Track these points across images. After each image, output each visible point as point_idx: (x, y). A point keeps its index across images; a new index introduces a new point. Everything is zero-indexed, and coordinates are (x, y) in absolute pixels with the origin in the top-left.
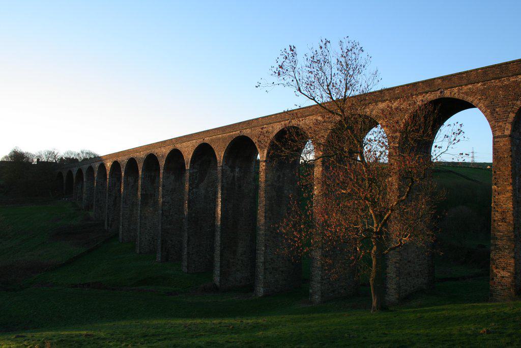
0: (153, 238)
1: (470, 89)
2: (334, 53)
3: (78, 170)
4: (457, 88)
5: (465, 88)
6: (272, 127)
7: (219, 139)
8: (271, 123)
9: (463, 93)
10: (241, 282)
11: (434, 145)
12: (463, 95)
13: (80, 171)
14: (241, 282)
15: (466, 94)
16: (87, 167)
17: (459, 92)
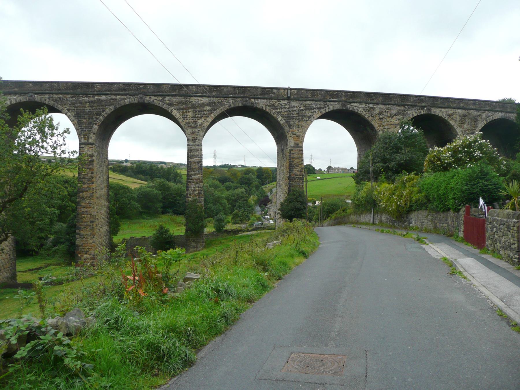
1: (60, 98)
4: (47, 95)
5: (56, 97)
9: (53, 100)
12: (53, 102)
16: (120, 232)
17: (49, 99)
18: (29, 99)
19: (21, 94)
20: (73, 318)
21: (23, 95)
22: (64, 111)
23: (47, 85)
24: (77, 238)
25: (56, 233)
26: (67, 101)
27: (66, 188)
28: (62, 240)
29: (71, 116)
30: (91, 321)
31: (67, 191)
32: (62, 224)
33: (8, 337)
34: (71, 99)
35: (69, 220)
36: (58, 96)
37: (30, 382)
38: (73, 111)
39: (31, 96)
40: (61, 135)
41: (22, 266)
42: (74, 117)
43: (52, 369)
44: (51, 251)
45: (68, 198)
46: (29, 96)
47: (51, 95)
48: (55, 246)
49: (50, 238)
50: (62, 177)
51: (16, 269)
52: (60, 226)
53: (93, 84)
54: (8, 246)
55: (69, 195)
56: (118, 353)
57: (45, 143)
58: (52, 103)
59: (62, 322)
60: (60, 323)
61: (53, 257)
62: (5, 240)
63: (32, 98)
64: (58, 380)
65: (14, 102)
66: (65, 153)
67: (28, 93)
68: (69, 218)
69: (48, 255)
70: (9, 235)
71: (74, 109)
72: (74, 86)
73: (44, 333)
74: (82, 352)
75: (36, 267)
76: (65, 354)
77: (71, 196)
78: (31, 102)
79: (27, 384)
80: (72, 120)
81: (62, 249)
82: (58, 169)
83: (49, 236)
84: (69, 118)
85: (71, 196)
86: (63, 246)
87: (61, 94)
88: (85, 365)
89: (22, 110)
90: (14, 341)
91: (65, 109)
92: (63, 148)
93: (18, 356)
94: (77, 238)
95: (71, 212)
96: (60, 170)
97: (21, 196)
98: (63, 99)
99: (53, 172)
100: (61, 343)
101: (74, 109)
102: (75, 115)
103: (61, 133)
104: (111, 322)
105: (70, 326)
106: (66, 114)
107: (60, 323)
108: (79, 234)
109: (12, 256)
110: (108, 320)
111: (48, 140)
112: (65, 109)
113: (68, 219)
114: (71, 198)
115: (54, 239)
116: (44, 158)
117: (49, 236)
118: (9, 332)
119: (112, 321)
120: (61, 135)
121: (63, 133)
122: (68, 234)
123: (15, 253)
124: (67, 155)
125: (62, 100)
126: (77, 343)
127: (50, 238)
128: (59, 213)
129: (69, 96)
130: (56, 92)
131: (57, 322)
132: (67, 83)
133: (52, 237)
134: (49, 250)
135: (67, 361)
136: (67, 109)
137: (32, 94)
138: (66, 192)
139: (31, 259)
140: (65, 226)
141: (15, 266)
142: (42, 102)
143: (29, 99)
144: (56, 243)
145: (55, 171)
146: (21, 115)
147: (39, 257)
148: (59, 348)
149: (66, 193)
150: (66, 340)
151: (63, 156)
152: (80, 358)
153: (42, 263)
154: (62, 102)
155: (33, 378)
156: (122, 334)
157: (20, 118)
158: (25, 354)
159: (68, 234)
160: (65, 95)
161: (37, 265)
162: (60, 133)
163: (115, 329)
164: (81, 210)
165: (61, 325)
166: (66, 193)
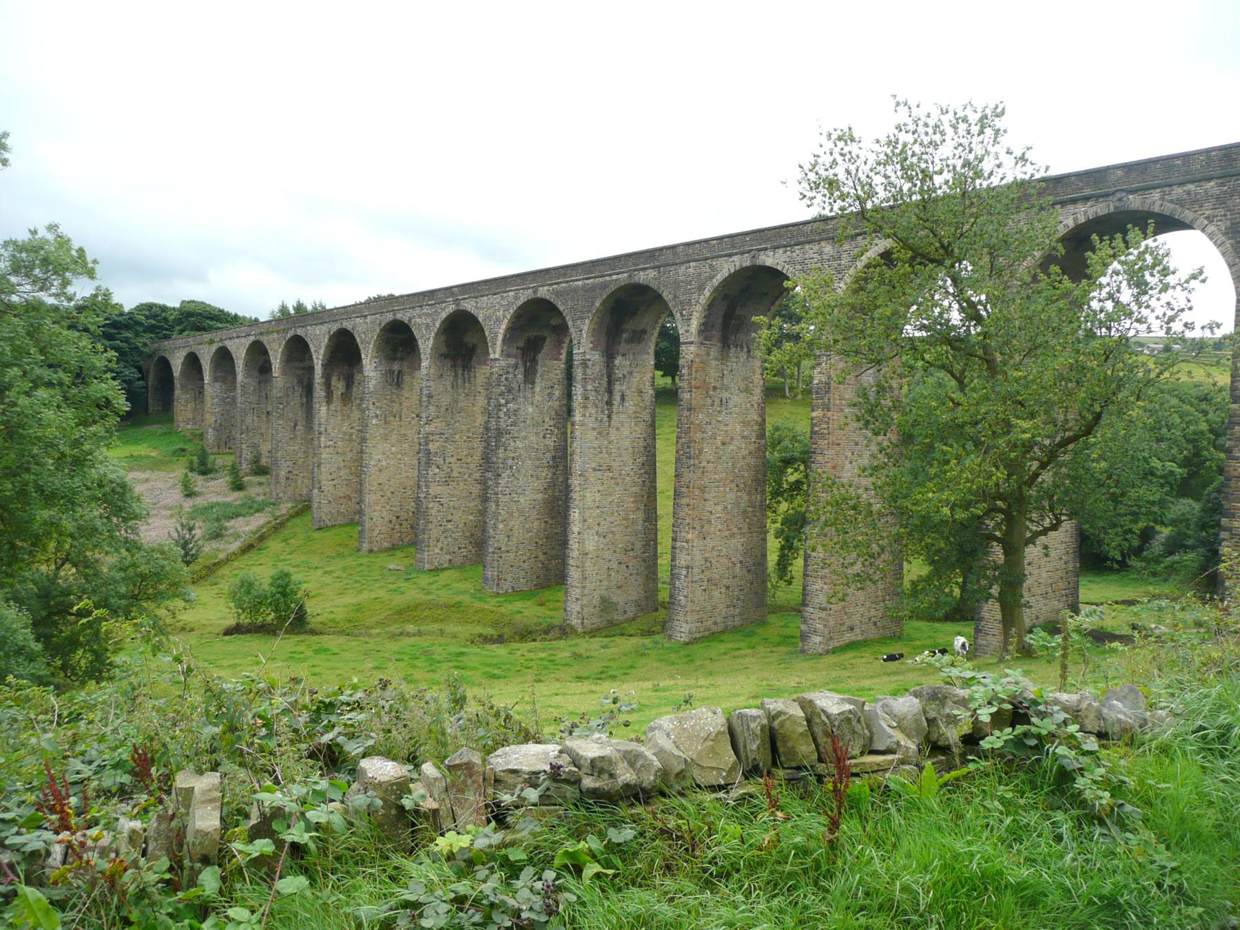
0: (398, 517)
1: (1189, 193)
2: (1166, 247)
3: (186, 357)
4: (1158, 190)
5: (1178, 191)
6: (711, 266)
7: (575, 290)
8: (706, 259)
9: (1171, 201)
10: (625, 612)
11: (1026, 562)
12: (1171, 206)
13: (258, 351)
14: (625, 612)
15: (1180, 202)
16: (172, 362)
17: (1162, 199)
18: (1116, 208)
19: (1097, 197)
20: (1120, 705)
21: (1101, 200)
22: (1198, 222)
23: (1158, 166)
24: (1224, 540)
25: (1173, 522)
26: (1207, 196)
27: (1205, 413)
28: (1190, 542)
29: (1217, 232)
30: (1162, 720)
31: (1207, 421)
32: (1191, 501)
33: (973, 706)
34: (1216, 191)
35: (1209, 495)
36: (1185, 188)
37: (1002, 800)
38: (1221, 220)
39: (1120, 200)
40: (1184, 285)
41: (1093, 590)
42: (1225, 234)
43: (1053, 792)
44: (1162, 565)
45: (1209, 439)
46: (1115, 199)
47: (1167, 189)
48: (1171, 553)
49: (1158, 533)
50: (1196, 386)
51: (1078, 597)
52: (1187, 507)
53: (1186, 157)
54: (1062, 542)
55: (1211, 431)
56: (1214, 808)
57: (1145, 312)
58: (1168, 209)
59: (1090, 705)
60: (1084, 705)
61: (1166, 580)
62: (1054, 527)
63: (1122, 204)
64: (1059, 816)
65: (1082, 220)
66: (1193, 329)
67: (1113, 193)
68: (1210, 489)
69: (1154, 574)
70: (1063, 518)
71: (1225, 215)
72: (1225, 155)
73: (1043, 715)
74: (1122, 778)
75: (1126, 598)
76: (1081, 769)
77: (1217, 435)
78: (1120, 212)
79: (996, 803)
80: (1219, 242)
81: (1188, 563)
82: (1175, 369)
83: (1158, 528)
84: (1211, 239)
85: (1217, 435)
86: (1191, 555)
87: (1193, 182)
88: (1123, 804)
89: (1095, 237)
90: (985, 715)
91: (1201, 219)
92: (1186, 317)
93: (985, 744)
94: (1224, 540)
95: (1214, 474)
96: (1179, 371)
97: (1089, 430)
98: (1196, 194)
99: (1162, 377)
100: (1071, 742)
101: (1225, 215)
102: (1226, 228)
103: (1182, 281)
104: (1208, 734)
105: (1107, 717)
106: (1203, 230)
107: (1084, 705)
108: (1229, 530)
109: (1071, 567)
110: (1201, 728)
111: (1153, 302)
112: (1201, 219)
113: (1206, 492)
114: (1216, 440)
115: (1169, 538)
116: (1157, 340)
117: (1158, 528)
118: (977, 696)
119: (1212, 733)
120: (1184, 285)
121: (1187, 282)
122: (1203, 527)
123: (1078, 559)
124: (1196, 334)
125: (1193, 196)
126: (1117, 759)
127: (1158, 533)
128: (1185, 475)
129: (1212, 183)
130: (1181, 179)
131: (1079, 701)
132: (1207, 152)
133: (1165, 532)
134: (1157, 561)
135: (1080, 783)
136: (1205, 218)
137: (1123, 194)
138: (1204, 424)
139: (1113, 577)
140: (1197, 506)
141: (1076, 588)
142: (1146, 208)
143: (1116, 208)
144: (1174, 546)
145: (1166, 374)
146: (1093, 250)
147: (1132, 576)
148: (1066, 753)
149: (1204, 426)
150: (1092, 744)
151: (1189, 334)
152: (1105, 784)
153: (1139, 590)
154: (1193, 202)
155: (1009, 795)
156: (1232, 768)
157: (1092, 258)
158: (999, 744)
159: (1203, 527)
160: (1202, 183)
161: (1128, 593)
162: (1180, 280)
163: (1217, 753)
164: (1235, 470)
165: (1086, 709)
166: (1204, 426)
